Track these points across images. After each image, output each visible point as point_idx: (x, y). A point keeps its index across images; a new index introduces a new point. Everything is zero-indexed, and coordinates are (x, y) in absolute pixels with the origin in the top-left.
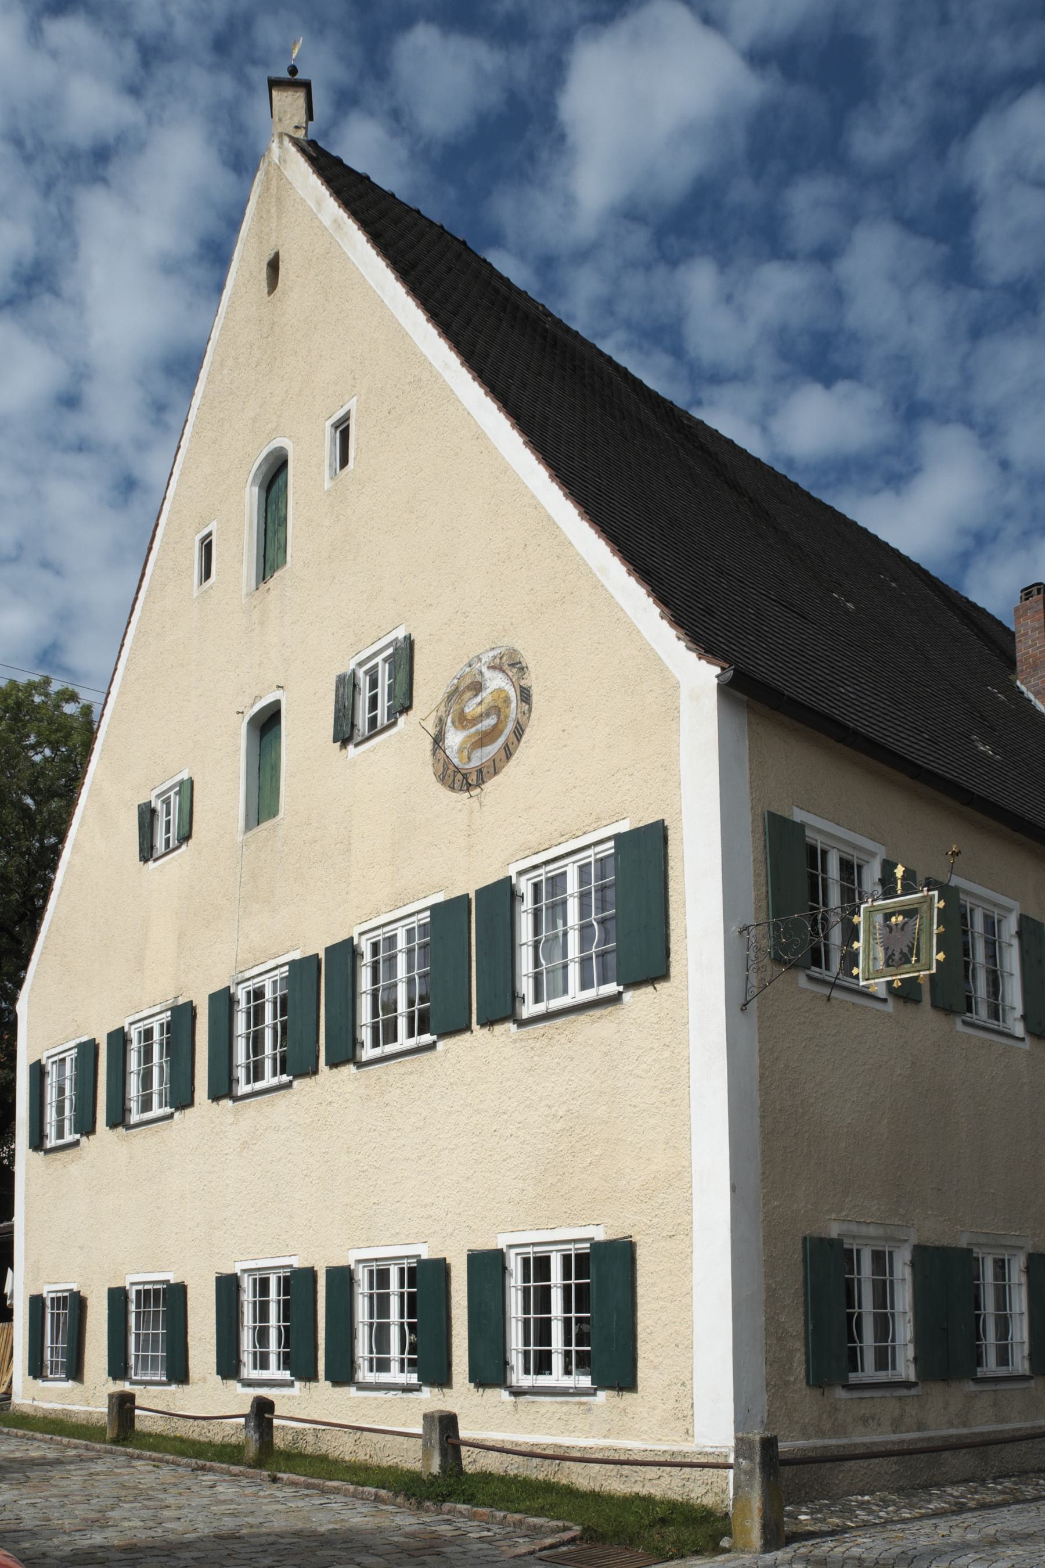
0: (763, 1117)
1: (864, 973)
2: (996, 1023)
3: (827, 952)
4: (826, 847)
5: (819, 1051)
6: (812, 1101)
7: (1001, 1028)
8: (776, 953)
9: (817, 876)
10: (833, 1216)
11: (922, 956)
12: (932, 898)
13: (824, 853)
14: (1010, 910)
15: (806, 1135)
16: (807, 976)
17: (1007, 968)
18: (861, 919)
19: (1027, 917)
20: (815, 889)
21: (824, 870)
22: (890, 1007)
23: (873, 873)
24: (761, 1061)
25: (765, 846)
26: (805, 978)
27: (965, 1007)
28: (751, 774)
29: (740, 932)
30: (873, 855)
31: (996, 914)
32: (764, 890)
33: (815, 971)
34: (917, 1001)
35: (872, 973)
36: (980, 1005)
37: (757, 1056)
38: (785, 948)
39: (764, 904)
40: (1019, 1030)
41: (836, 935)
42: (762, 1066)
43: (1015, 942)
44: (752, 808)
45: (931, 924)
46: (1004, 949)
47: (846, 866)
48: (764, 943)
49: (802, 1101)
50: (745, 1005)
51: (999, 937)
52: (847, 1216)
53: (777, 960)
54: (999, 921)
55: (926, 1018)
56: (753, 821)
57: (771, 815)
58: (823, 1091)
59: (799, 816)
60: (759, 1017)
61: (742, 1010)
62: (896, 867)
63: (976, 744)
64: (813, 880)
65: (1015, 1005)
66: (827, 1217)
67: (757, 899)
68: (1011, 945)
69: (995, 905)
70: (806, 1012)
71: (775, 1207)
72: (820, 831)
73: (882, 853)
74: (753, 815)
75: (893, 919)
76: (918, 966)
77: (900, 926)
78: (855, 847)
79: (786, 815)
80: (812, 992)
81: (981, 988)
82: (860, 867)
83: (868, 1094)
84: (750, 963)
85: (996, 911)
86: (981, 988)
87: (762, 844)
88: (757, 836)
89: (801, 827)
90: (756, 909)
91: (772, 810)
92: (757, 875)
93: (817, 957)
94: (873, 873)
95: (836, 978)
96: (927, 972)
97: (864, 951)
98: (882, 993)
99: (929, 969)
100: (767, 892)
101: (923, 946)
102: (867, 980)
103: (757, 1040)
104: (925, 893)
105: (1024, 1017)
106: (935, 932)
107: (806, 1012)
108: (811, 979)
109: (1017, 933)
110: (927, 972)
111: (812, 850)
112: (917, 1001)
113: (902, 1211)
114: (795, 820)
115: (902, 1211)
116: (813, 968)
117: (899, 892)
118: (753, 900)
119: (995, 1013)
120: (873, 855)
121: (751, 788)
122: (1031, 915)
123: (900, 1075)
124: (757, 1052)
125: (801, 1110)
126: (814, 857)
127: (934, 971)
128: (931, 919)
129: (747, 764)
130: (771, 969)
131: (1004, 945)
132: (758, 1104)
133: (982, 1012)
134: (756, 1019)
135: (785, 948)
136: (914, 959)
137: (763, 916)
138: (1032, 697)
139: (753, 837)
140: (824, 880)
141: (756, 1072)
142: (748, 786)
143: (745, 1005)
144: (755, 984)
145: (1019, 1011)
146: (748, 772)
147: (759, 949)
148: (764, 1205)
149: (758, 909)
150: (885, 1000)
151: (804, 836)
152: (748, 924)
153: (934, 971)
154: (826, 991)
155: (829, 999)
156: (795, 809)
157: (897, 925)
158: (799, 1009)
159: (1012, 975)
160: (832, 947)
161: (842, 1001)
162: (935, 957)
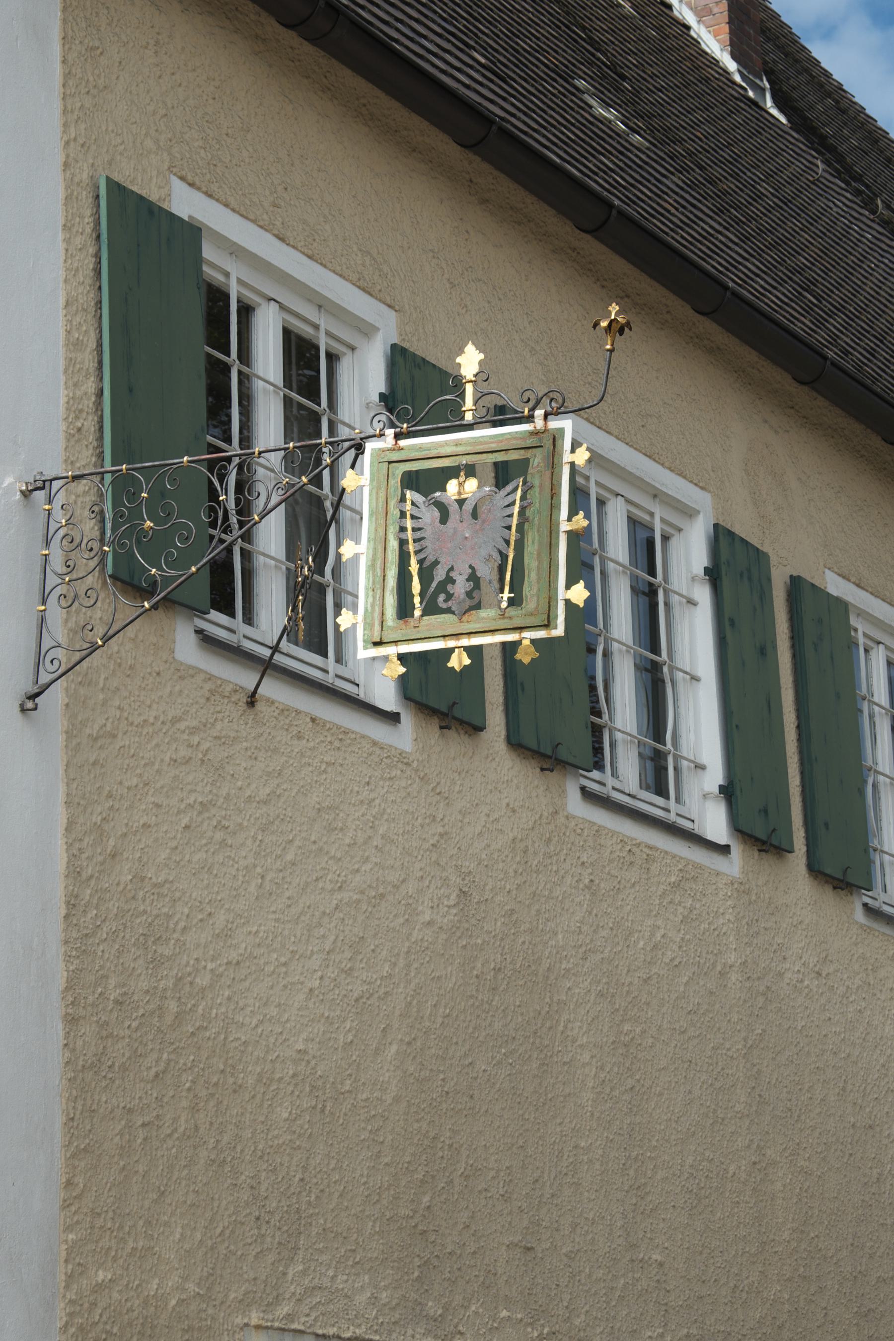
0: (71, 1021)
1: (369, 625)
2: (660, 801)
3: (248, 575)
4: (251, 297)
5: (223, 843)
6: (203, 980)
7: (672, 817)
8: (124, 559)
9: (227, 368)
10: (255, 1318)
11: (530, 590)
12: (556, 438)
13: (246, 311)
14: (690, 513)
15: (187, 1079)
16: (199, 632)
17: (683, 660)
18: (365, 479)
19: (731, 534)
20: (220, 397)
21: (245, 355)
22: (406, 736)
23: (362, 380)
24: (72, 858)
25: (98, 272)
26: (192, 638)
27: (591, 759)
28: (67, 75)
29: (26, 494)
30: (367, 330)
31: (659, 518)
32: (90, 386)
33: (217, 622)
34: (475, 728)
35: (371, 644)
36: (620, 750)
37: (60, 843)
38: (155, 545)
39: (89, 423)
40: (715, 823)
41: (271, 535)
42: (74, 872)
43: (703, 595)
44: (66, 165)
45: (554, 507)
46: (676, 611)
47: (300, 354)
48: (90, 528)
49: (179, 980)
50: (33, 697)
51: (666, 579)
52: (290, 1317)
53: (129, 582)
54: (666, 538)
55: (492, 772)
56: (68, 199)
57: (117, 190)
58: (234, 956)
59: (185, 203)
60: (69, 735)
61: (23, 710)
62: (461, 351)
63: (586, 97)
64: (217, 374)
65: (704, 760)
66: (239, 1320)
67: (73, 410)
68: (692, 602)
69: (656, 495)
70: (193, 731)
71: (99, 1288)
72: (236, 251)
73: (388, 329)
74: (70, 184)
75: (452, 486)
76: (517, 616)
77: (468, 507)
78: (322, 304)
79: (153, 195)
80: (210, 677)
81: (625, 711)
82: (332, 358)
83: (349, 972)
84: (52, 580)
85: (659, 512)
86: (625, 711)
87: (90, 263)
88: (78, 241)
89: (191, 233)
90: (69, 437)
91: (117, 177)
92: (74, 345)
93: (224, 587)
94: (362, 380)
95: (275, 649)
96: (541, 634)
97: (372, 567)
98: (385, 695)
99: (547, 626)
100: (100, 393)
101: (531, 562)
102: (377, 644)
103: (61, 797)
104: (539, 423)
105: (727, 792)
106: (565, 526)
107: (193, 731)
108: (207, 640)
109: (707, 571)
110: (541, 634)
111: (216, 298)
112: (474, 728)
113: (433, 1308)
114: (176, 210)
115: (433, 1308)
116: (215, 615)
117: (469, 417)
118: (62, 409)
119: (658, 774)
120: (367, 330)
121: (65, 111)
122: (738, 530)
123: (430, 923)
124: (60, 830)
125: (173, 1006)
126: (220, 318)
127: (559, 631)
128: (554, 494)
129: (56, 49)
130: (108, 606)
131: (675, 599)
132: (60, 981)
133: (626, 772)
134: (61, 739)
135: (155, 545)
136: (506, 595)
137: (85, 460)
138: (690, 18)
139: (68, 241)
140: (244, 379)
141: (57, 890)
142: (57, 105)
143: (33, 697)
144: (62, 638)
145: (715, 775)
146: (58, 70)
147: (72, 544)
148: (70, 1278)
149: (74, 435)
150: (393, 718)
151: (198, 260)
152: (48, 475)
153: (559, 631)
154: (247, 679)
155: (252, 700)
156: (177, 185)
157: (461, 502)
158: (175, 720)
159: (695, 679)
160: (259, 561)
161: (285, 710)
162: (562, 594)
